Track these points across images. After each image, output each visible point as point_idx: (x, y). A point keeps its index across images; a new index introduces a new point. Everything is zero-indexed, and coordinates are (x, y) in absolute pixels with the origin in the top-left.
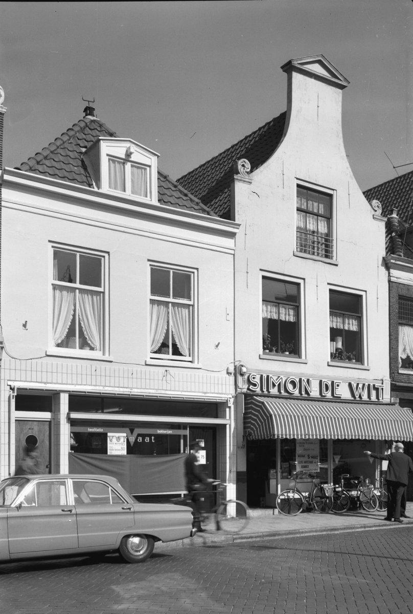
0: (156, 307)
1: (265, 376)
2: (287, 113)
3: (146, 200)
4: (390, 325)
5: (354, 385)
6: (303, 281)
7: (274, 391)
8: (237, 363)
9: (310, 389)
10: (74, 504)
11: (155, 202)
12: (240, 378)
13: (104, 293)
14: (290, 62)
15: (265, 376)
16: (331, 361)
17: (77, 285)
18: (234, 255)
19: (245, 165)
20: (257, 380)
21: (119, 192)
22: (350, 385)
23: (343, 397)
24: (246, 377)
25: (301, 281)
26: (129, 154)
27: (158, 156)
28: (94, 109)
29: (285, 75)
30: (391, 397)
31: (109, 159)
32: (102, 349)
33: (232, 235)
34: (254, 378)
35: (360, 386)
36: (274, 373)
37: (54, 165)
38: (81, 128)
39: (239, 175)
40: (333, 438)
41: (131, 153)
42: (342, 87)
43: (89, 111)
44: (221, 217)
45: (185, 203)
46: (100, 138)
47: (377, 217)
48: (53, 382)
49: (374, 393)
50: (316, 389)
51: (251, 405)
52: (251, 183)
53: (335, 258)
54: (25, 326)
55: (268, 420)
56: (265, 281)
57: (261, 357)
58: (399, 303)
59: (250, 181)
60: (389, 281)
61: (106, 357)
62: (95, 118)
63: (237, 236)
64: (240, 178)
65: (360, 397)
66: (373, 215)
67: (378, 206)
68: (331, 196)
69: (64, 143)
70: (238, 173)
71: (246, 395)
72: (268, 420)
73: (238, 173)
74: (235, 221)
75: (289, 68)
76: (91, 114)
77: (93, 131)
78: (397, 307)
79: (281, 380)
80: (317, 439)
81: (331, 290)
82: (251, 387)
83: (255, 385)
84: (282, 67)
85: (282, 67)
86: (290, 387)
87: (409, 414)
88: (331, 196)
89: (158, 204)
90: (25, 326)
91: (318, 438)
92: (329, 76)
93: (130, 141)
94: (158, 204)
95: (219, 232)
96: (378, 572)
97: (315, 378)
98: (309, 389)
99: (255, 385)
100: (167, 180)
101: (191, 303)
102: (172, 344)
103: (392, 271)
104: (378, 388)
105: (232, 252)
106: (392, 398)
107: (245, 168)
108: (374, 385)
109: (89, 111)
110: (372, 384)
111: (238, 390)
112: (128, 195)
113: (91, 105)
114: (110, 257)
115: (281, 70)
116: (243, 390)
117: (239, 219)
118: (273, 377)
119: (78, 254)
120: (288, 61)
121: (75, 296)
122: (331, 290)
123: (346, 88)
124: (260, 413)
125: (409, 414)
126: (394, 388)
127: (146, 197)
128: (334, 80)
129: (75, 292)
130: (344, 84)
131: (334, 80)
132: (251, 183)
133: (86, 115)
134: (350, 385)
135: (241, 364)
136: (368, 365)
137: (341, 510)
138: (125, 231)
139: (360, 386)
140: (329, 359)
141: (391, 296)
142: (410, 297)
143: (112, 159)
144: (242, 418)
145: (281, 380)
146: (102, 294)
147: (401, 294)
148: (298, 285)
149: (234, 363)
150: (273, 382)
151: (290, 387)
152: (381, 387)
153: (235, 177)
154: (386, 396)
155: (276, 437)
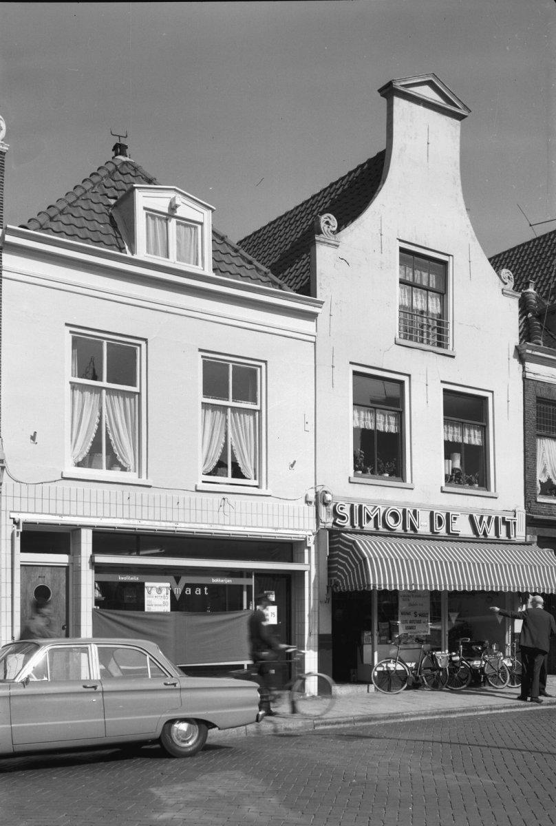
0: (209, 413)
1: (356, 505)
2: (387, 152)
3: (197, 270)
4: (524, 438)
5: (477, 519)
6: (408, 378)
7: (369, 526)
8: (319, 489)
9: (417, 523)
10: (99, 678)
11: (208, 272)
12: (323, 509)
13: (139, 394)
14: (390, 84)
15: (356, 505)
16: (446, 485)
17: (104, 383)
18: (315, 343)
19: (330, 222)
20: (347, 511)
21: (161, 258)
22: (471, 518)
23: (462, 534)
24: (331, 507)
25: (405, 379)
26: (173, 208)
27: (213, 210)
28: (126, 147)
29: (384, 100)
30: (526, 534)
31: (147, 215)
32: (137, 469)
33: (312, 316)
34: (342, 509)
35: (485, 519)
36: (369, 502)
38: (109, 172)
39: (322, 235)
40: (448, 589)
41: (177, 206)
42: (460, 117)
43: (120, 149)
44: (297, 291)
45: (249, 273)
46: (135, 185)
47: (508, 292)
48: (72, 513)
49: (503, 529)
50: (426, 524)
51: (337, 545)
52: (337, 246)
53: (450, 347)
54: (33, 438)
55: (361, 566)
56: (357, 377)
57: (351, 481)
58: (537, 407)
59: (336, 243)
60: (524, 378)
61: (143, 481)
62: (127, 159)
63: (319, 318)
64: (323, 240)
65: (485, 534)
66: (502, 290)
67: (509, 278)
68: (445, 263)
69: (86, 192)
70: (320, 232)
71: (331, 532)
72: (361, 566)
73: (320, 232)
74: (316, 297)
75: (389, 91)
76: (123, 153)
77: (125, 176)
78: (535, 413)
79: (378, 512)
81: (445, 391)
82: (338, 521)
83: (343, 518)
84: (380, 91)
85: (380, 91)
86: (390, 521)
87: (551, 557)
88: (445, 263)
89: (213, 275)
90: (33, 438)
93: (175, 190)
94: (213, 275)
97: (424, 508)
98: (416, 524)
99: (343, 518)
100: (225, 242)
101: (257, 407)
102: (232, 463)
103: (527, 364)
104: (509, 522)
105: (313, 339)
106: (528, 536)
107: (330, 226)
108: (503, 518)
109: (120, 149)
110: (500, 517)
111: (321, 524)
112: (172, 262)
113: (123, 141)
115: (379, 95)
116: (327, 525)
117: (321, 294)
118: (367, 507)
119: (105, 342)
120: (388, 82)
122: (445, 391)
123: (466, 118)
124: (349, 555)
125: (551, 557)
126: (531, 522)
127: (197, 264)
128: (449, 107)
129: (101, 393)
130: (464, 112)
131: (449, 107)
132: (337, 246)
133: (116, 155)
134: (471, 518)
135: (325, 489)
136: (495, 491)
137: (458, 687)
139: (485, 519)
140: (443, 483)
141: (527, 398)
142: (552, 400)
143: (151, 213)
144: (326, 563)
145: (378, 512)
146: (137, 396)
147: (539, 395)
149: (315, 488)
150: (367, 514)
151: (390, 521)
152: (513, 521)
153: (317, 238)
154: (520, 533)
155: (372, 588)
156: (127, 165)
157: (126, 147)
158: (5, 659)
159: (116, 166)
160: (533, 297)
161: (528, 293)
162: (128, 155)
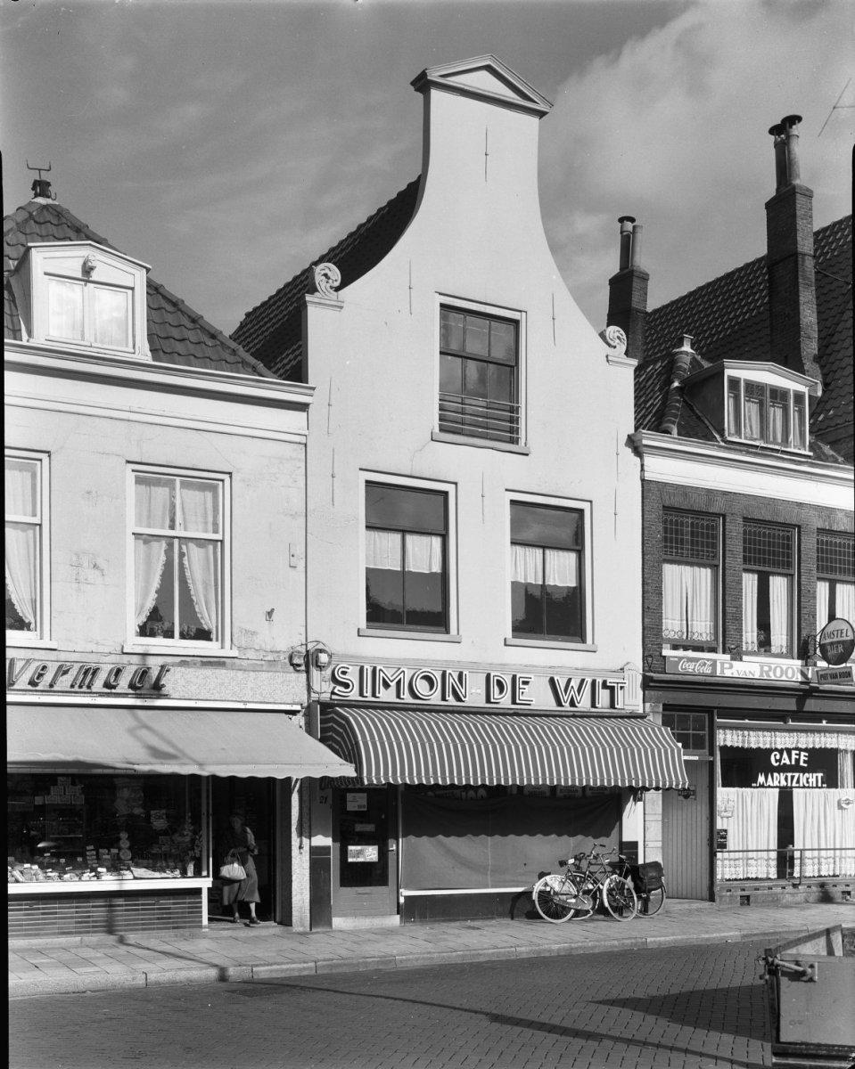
1: (368, 668)
3: (126, 350)
4: (643, 565)
5: (562, 684)
6: (454, 486)
7: (387, 696)
8: (310, 646)
9: (463, 691)
11: (144, 355)
12: (315, 673)
13: (222, 541)
14: (423, 75)
15: (368, 668)
16: (368, 627)
18: (306, 445)
19: (329, 274)
20: (353, 676)
22: (552, 681)
23: (536, 705)
24: (328, 672)
25: (585, 506)
26: (87, 270)
27: (148, 270)
28: (48, 184)
29: (420, 96)
30: (644, 702)
32: (220, 638)
33: (303, 407)
34: (344, 673)
35: (575, 684)
36: (388, 662)
37: (170, 335)
39: (317, 294)
40: (518, 783)
41: (92, 269)
42: (541, 114)
44: (280, 377)
45: (209, 352)
47: (616, 359)
49: (604, 696)
50: (479, 691)
51: (331, 724)
52: (341, 307)
53: (522, 442)
54: (270, 614)
57: (508, 643)
58: (665, 522)
59: (339, 304)
60: (643, 480)
61: (46, 643)
62: (49, 201)
63: (311, 409)
64: (316, 300)
65: (572, 704)
66: (607, 356)
67: (618, 338)
68: (516, 323)
70: (313, 290)
71: (326, 707)
73: (313, 290)
74: (307, 383)
75: (423, 84)
76: (44, 194)
78: (661, 529)
79: (402, 676)
80: (544, 784)
82: (338, 688)
83: (346, 686)
84: (413, 83)
85: (413, 83)
86: (422, 687)
88: (516, 323)
90: (270, 614)
91: (548, 783)
92: (519, 98)
93: (90, 245)
94: (676, 436)
95: (203, 393)
96: (641, 1022)
97: (474, 667)
98: (461, 692)
99: (346, 686)
100: (179, 310)
101: (218, 537)
103: (648, 460)
104: (614, 687)
105: (303, 440)
106: (648, 705)
107: (330, 281)
108: (605, 682)
110: (600, 681)
111: (313, 695)
113: (45, 177)
114: (233, 480)
115: (412, 88)
116: (324, 695)
118: (452, 673)
120: (419, 73)
121: (207, 553)
123: (547, 115)
124: (343, 738)
126: (647, 684)
130: (541, 107)
132: (341, 307)
133: (36, 195)
134: (552, 681)
135: (320, 646)
136: (593, 643)
137: (552, 918)
138: (131, 419)
139: (575, 684)
140: (509, 633)
141: (646, 508)
145: (402, 676)
146: (38, 527)
147: (667, 504)
148: (581, 512)
149: (306, 645)
150: (384, 679)
151: (422, 687)
152: (620, 685)
153: (308, 298)
155: (366, 783)
156: (48, 210)
157: (48, 184)
158: (782, 1050)
159: (29, 213)
160: (688, 359)
161: (681, 353)
162: (53, 196)
